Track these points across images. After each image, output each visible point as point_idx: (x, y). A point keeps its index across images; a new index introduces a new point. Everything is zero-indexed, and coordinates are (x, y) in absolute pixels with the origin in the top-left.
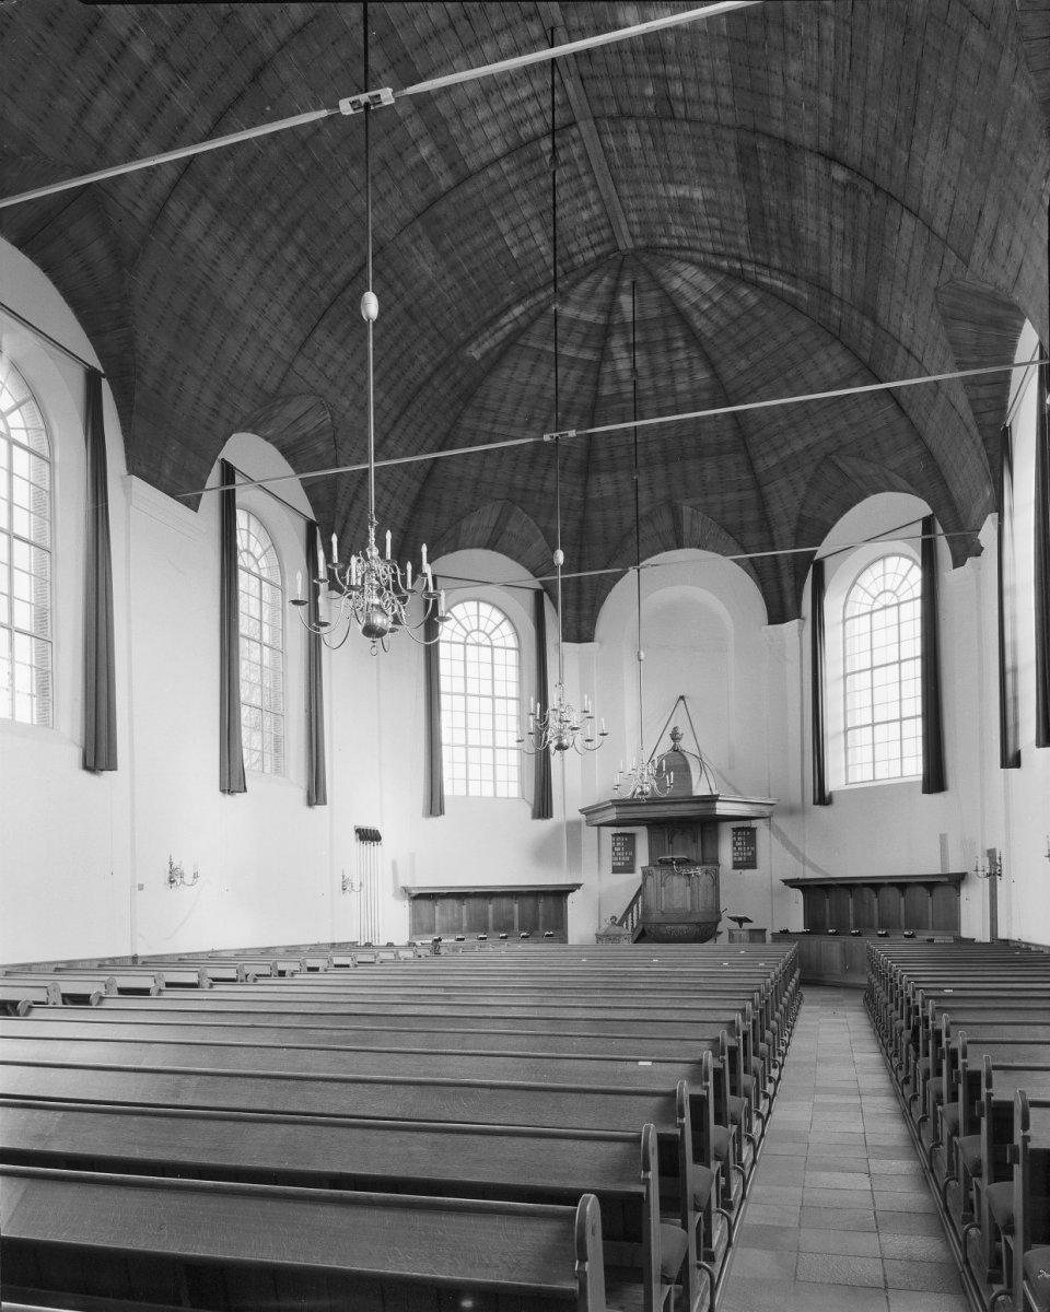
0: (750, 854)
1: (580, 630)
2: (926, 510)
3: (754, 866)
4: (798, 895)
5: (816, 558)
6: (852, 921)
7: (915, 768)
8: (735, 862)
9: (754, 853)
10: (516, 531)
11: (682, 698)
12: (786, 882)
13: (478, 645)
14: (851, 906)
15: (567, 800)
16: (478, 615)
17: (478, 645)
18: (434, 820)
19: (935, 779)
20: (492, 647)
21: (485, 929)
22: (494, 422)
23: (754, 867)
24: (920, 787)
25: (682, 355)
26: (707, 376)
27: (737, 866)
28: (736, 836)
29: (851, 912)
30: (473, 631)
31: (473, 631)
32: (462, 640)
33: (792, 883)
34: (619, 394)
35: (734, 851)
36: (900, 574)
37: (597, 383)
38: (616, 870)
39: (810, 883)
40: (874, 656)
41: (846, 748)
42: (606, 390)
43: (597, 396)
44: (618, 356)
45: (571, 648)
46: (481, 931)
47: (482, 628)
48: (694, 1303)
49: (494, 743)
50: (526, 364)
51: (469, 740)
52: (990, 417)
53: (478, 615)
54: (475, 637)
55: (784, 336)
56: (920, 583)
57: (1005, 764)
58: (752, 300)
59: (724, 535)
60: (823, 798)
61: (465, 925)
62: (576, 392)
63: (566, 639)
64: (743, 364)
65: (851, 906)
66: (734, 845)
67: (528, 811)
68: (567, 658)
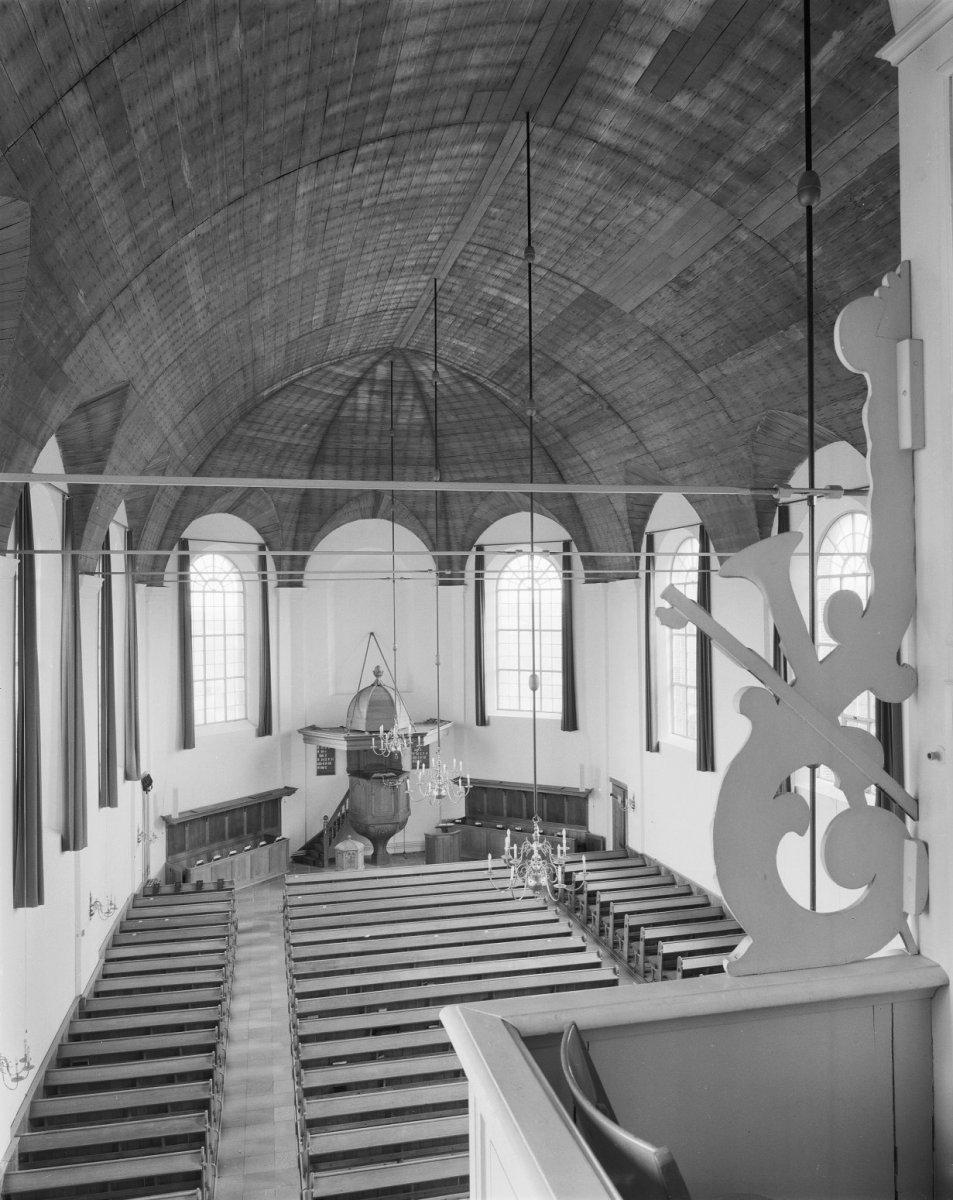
1: (293, 574)
2: (567, 536)
6: (505, 812)
7: (552, 705)
10: (253, 503)
11: (372, 634)
13: (214, 591)
14: (504, 800)
15: (283, 720)
17: (214, 591)
18: (188, 751)
19: (570, 722)
20: (224, 592)
21: (222, 837)
22: (259, 430)
24: (560, 726)
25: (408, 403)
26: (421, 417)
29: (505, 805)
32: (201, 589)
34: (354, 417)
37: (339, 408)
38: (320, 773)
41: (498, 683)
42: (345, 413)
43: (336, 415)
44: (362, 395)
45: (286, 592)
50: (294, 396)
52: (638, 522)
54: (211, 586)
55: (489, 414)
57: (649, 748)
58: (474, 390)
59: (413, 518)
60: (482, 720)
61: (208, 838)
62: (323, 413)
64: (452, 418)
65: (504, 800)
67: (254, 733)
68: (283, 599)
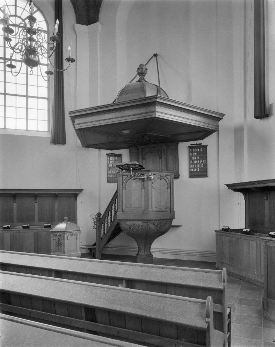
0: (202, 166)
3: (206, 176)
4: (240, 198)
5: (243, 231)
8: (190, 172)
9: (206, 165)
11: (155, 55)
12: (231, 186)
16: (16, 6)
23: (206, 176)
27: (192, 175)
28: (192, 152)
30: (20, 17)
31: (20, 17)
33: (234, 187)
35: (190, 164)
36: (158, 108)
39: (251, 186)
40: (1, 36)
45: (82, 28)
46: (6, 222)
47: (18, 14)
48: (211, 300)
49: (16, 85)
51: (17, 82)
53: (16, 6)
56: (77, 137)
63: (79, 21)
66: (190, 158)
